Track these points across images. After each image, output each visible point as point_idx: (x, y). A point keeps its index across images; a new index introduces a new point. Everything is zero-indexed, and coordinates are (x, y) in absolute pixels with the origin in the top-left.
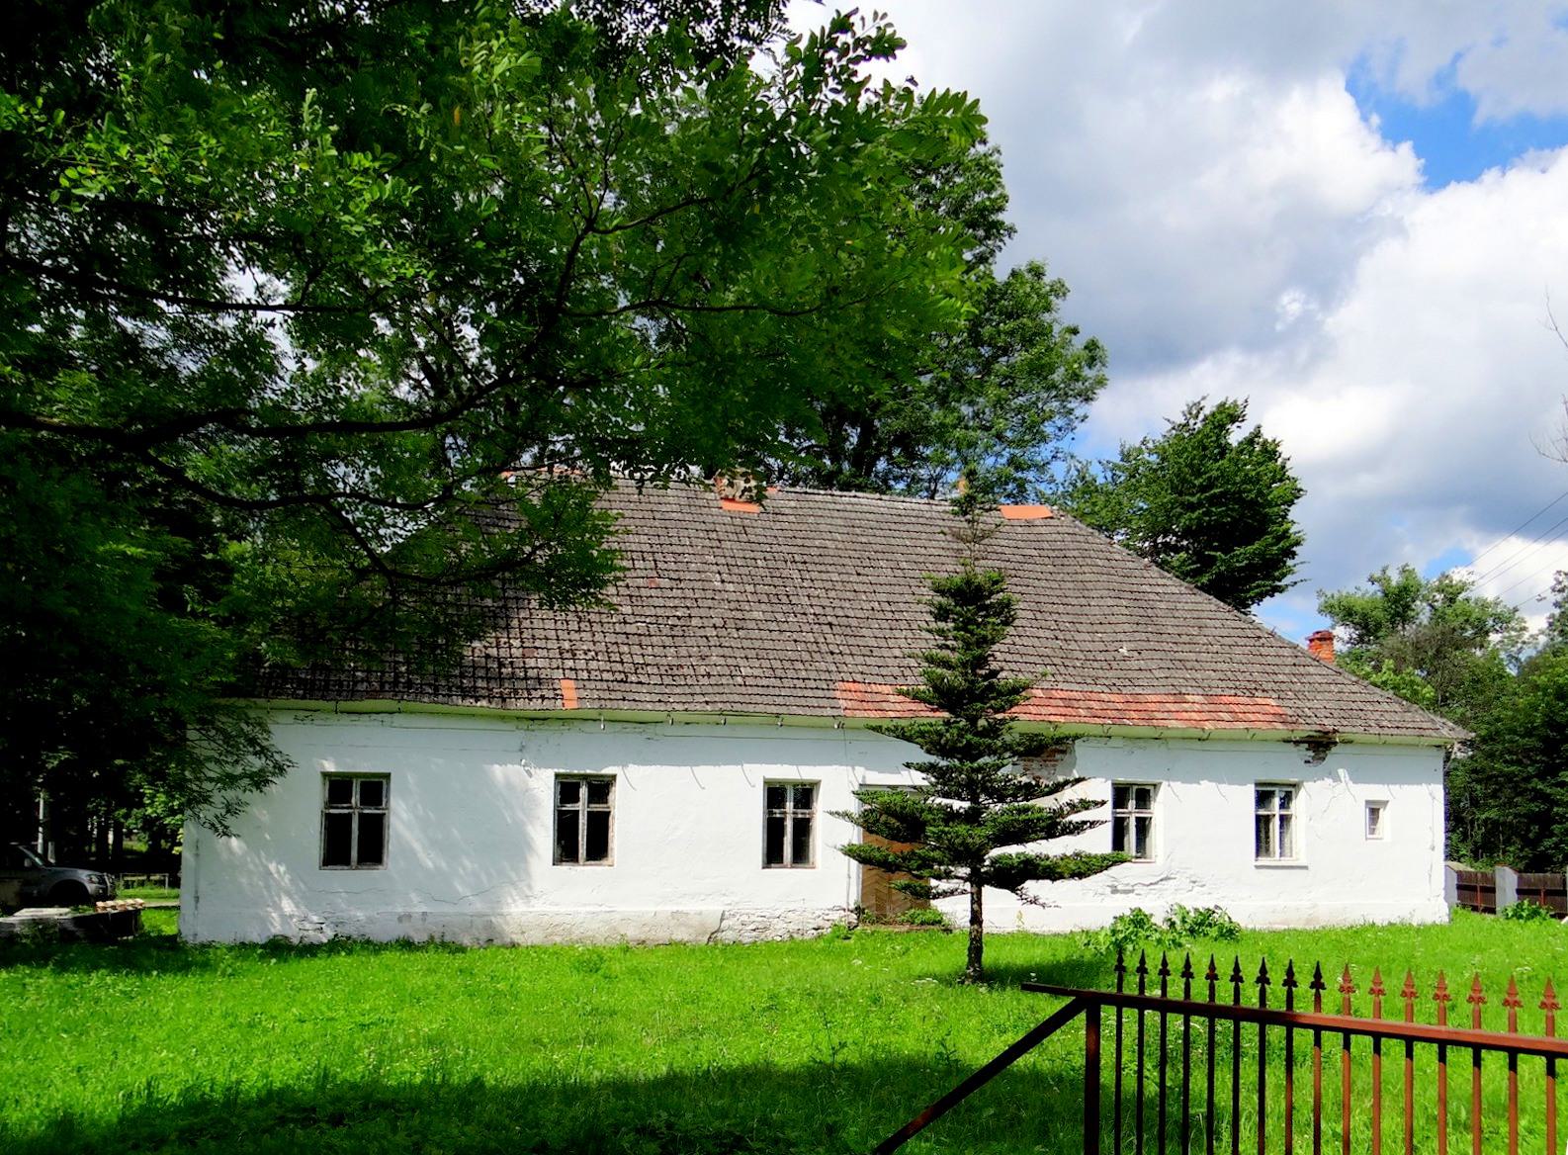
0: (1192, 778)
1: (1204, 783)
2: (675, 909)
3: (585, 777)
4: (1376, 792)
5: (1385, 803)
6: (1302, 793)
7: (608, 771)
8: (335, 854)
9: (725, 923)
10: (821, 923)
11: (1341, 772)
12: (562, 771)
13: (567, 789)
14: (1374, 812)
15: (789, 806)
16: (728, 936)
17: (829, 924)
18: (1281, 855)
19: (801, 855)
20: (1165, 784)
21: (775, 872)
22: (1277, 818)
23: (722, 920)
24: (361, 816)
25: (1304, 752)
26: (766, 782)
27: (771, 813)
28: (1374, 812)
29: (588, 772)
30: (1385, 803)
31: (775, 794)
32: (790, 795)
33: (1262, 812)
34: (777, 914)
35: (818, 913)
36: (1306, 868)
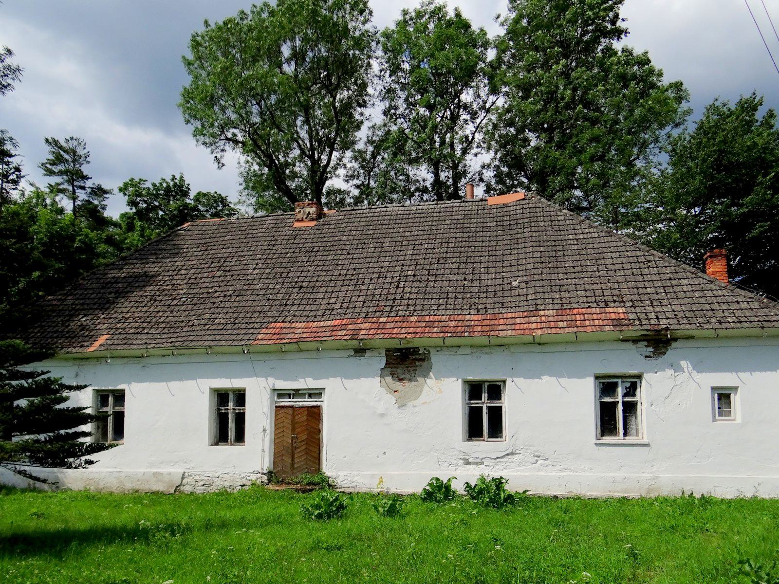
0: (534, 374)
1: (546, 378)
2: (155, 470)
3: (113, 391)
5: (735, 389)
7: (120, 387)
9: (185, 481)
10: (244, 481)
11: (683, 363)
12: (96, 388)
14: (724, 397)
15: (231, 405)
16: (187, 489)
17: (250, 483)
18: (625, 434)
19: (240, 437)
20: (646, 376)
21: (223, 448)
22: (620, 407)
23: (183, 478)
24: (489, 408)
25: (644, 348)
27: (219, 410)
28: (724, 397)
29: (110, 388)
30: (735, 389)
31: (221, 396)
32: (231, 397)
33: (607, 399)
34: (217, 475)
35: (243, 475)
36: (647, 445)
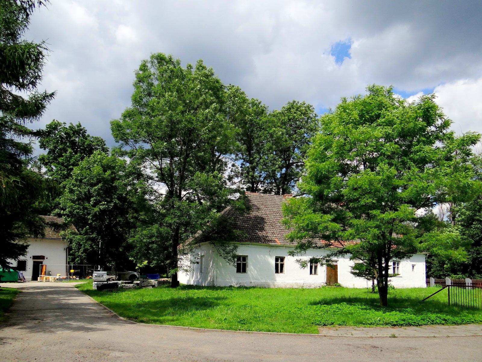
4: (414, 263)
5: (415, 265)
6: (401, 263)
8: (238, 271)
13: (277, 260)
21: (311, 275)
26: (276, 257)
30: (415, 265)
